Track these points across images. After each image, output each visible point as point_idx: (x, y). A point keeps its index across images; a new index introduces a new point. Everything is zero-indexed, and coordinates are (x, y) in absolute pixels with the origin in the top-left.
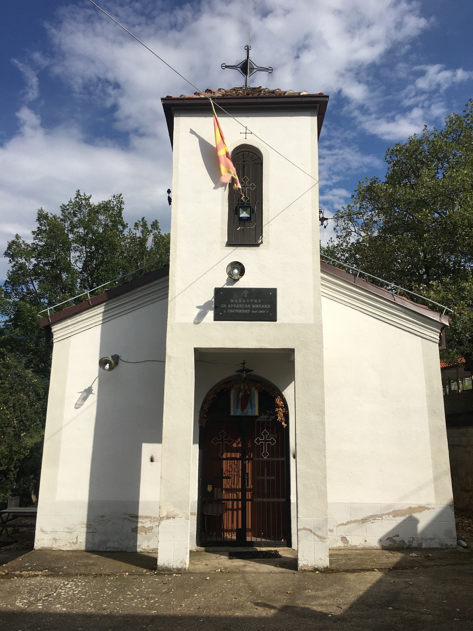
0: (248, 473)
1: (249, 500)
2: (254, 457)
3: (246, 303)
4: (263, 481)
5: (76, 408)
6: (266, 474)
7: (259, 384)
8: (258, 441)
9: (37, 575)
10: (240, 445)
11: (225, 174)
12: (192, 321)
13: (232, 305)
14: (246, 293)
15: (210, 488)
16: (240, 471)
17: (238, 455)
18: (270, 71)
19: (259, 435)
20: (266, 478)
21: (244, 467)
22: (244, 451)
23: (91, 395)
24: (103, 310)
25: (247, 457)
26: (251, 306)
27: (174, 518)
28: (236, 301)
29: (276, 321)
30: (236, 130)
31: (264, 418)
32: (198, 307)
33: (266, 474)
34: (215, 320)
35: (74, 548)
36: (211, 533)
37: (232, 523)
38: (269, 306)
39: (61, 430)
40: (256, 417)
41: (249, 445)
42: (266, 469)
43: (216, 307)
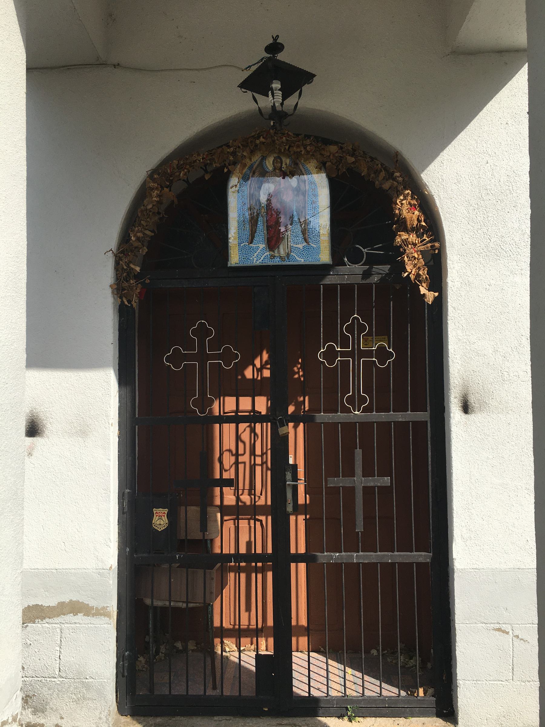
0: (295, 466)
1: (298, 558)
2: (315, 408)
4: (350, 491)
6: (359, 470)
7: (333, 148)
8: (331, 355)
10: (267, 373)
15: (160, 520)
16: (269, 452)
17: (262, 404)
19: (331, 336)
20: (359, 481)
21: (280, 446)
22: (278, 389)
25: (291, 409)
31: (351, 273)
33: (359, 470)
36: (179, 645)
37: (248, 609)
40: (324, 269)
41: (298, 373)
42: (359, 453)
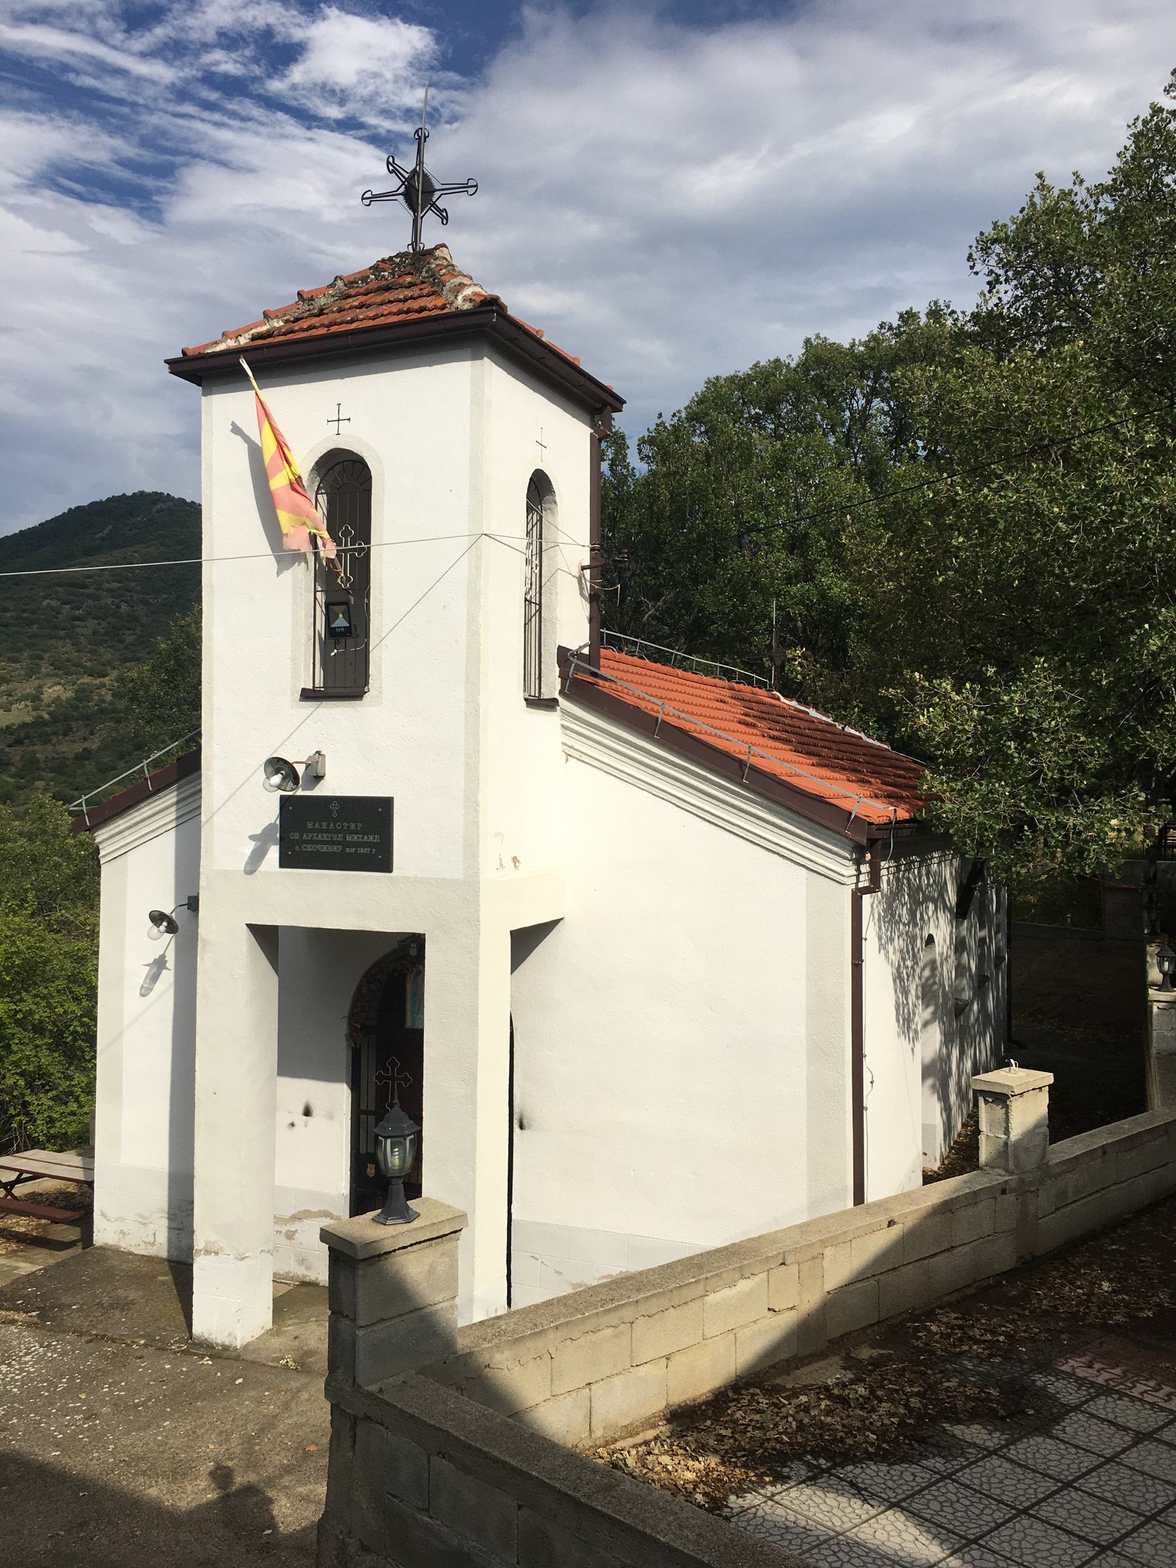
3: (338, 832)
5: (143, 995)
9: (13, 1322)
11: (292, 530)
12: (242, 867)
13: (310, 835)
14: (334, 807)
18: (471, 191)
23: (164, 971)
24: (175, 800)
26: (345, 837)
27: (216, 1253)
28: (317, 826)
29: (391, 871)
30: (314, 414)
32: (252, 838)
34: (281, 866)
35: (151, 1251)
38: (377, 839)
39: (121, 1034)
43: (281, 839)
